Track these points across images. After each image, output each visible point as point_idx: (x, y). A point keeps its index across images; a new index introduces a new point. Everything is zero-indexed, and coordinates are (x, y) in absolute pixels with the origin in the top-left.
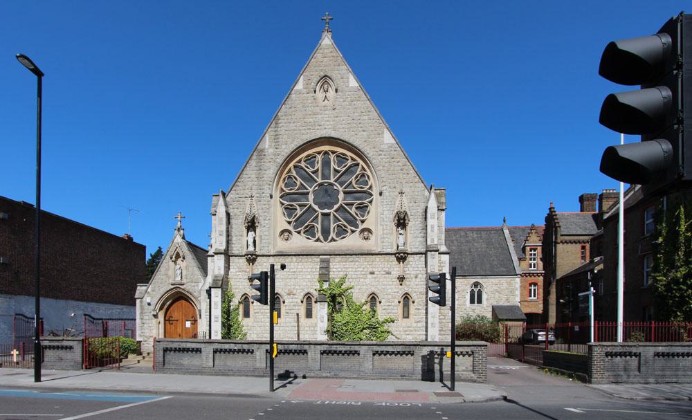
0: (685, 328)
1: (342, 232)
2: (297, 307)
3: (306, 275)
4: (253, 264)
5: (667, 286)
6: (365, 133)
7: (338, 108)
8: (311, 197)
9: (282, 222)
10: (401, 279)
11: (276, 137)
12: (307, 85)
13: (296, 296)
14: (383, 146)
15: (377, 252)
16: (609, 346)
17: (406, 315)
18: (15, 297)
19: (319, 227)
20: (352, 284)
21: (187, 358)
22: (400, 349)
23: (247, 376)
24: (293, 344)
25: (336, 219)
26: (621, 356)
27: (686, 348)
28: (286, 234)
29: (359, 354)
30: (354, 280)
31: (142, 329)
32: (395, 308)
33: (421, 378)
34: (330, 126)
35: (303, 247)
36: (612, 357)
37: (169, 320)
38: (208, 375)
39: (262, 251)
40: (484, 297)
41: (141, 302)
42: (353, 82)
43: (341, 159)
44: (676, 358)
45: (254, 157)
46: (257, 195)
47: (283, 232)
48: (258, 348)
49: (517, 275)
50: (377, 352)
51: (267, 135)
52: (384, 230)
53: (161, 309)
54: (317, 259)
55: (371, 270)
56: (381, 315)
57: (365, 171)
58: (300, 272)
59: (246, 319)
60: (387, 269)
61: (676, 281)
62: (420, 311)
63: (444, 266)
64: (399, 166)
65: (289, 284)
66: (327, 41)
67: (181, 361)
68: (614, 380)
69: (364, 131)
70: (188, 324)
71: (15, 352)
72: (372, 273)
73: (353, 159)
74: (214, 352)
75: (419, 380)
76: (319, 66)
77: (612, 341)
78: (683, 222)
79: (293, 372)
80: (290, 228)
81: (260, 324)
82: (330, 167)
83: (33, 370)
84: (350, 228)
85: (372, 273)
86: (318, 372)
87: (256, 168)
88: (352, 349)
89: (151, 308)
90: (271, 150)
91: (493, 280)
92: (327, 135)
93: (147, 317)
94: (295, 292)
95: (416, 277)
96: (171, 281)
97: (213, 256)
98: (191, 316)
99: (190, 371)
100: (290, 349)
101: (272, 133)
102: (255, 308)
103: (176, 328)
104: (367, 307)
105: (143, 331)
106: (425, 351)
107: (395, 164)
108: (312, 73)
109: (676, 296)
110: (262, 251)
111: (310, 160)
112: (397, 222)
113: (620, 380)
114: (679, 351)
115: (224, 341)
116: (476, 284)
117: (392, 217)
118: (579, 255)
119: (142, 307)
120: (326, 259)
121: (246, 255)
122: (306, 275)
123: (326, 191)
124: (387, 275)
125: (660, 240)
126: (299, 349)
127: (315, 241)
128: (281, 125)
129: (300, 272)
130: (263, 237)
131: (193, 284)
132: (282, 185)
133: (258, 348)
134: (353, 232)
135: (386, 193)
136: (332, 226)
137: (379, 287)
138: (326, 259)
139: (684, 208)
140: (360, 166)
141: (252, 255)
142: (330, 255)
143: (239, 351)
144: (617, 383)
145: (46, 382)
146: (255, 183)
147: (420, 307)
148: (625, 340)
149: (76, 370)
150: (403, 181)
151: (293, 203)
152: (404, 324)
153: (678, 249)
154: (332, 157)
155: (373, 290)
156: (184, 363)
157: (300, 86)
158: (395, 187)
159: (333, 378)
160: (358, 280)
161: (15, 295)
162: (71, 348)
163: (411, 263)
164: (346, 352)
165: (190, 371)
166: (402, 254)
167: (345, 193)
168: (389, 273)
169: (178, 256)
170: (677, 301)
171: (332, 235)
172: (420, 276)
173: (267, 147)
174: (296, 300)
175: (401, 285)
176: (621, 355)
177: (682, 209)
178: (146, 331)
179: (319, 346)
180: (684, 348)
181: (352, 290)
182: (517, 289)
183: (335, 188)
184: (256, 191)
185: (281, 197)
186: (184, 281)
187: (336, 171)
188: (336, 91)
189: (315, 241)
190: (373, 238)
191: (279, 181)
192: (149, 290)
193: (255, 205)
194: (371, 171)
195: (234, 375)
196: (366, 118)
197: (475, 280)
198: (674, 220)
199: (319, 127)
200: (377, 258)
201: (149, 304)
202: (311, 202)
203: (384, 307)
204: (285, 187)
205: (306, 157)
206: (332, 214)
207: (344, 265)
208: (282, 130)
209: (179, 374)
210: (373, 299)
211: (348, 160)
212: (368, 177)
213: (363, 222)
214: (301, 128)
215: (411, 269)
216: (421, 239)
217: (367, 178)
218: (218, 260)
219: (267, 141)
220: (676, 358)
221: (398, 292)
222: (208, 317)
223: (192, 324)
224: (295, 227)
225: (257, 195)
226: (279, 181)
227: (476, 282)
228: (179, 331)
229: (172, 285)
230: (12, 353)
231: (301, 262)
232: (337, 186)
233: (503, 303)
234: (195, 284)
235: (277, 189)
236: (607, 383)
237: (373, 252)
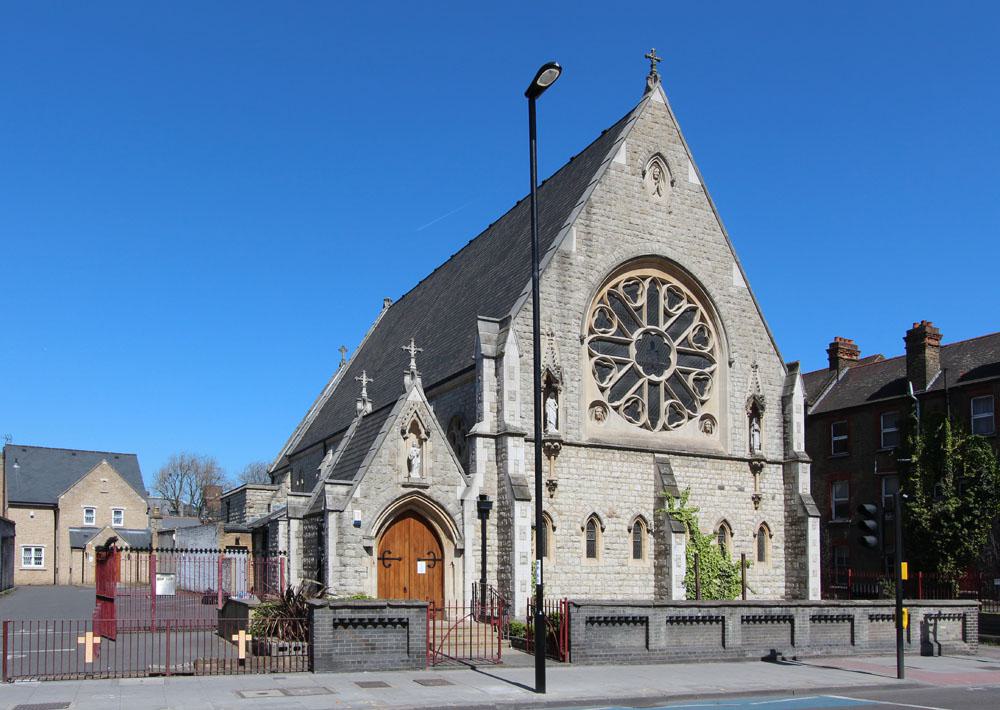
0: (957, 577)
1: (675, 415)
2: (622, 540)
3: (634, 484)
5: (935, 522)
6: (709, 263)
7: (675, 212)
9: (590, 389)
10: (757, 499)
11: (588, 238)
12: (632, 159)
13: (621, 520)
14: (732, 290)
15: (726, 455)
17: (761, 557)
19: (646, 402)
20: (697, 503)
21: (619, 636)
22: (759, 612)
23: (716, 661)
24: (775, 606)
25: (668, 395)
28: (600, 409)
30: (699, 498)
31: (341, 577)
32: (750, 544)
33: (919, 651)
34: (665, 240)
37: (435, 560)
38: (658, 663)
39: (569, 437)
41: (340, 519)
42: (694, 178)
43: (674, 296)
46: (561, 334)
47: (594, 404)
48: (731, 614)
50: (342, 621)
51: (574, 229)
54: (648, 458)
55: (719, 482)
57: (707, 322)
58: (626, 478)
60: (739, 483)
61: (945, 515)
62: (778, 550)
64: (751, 325)
65: (611, 498)
66: (657, 96)
67: (610, 641)
69: (708, 259)
70: (422, 567)
71: (89, 640)
72: (721, 488)
73: (690, 301)
75: (916, 654)
76: (648, 134)
78: (949, 440)
79: (780, 654)
80: (604, 398)
81: (566, 568)
82: (658, 306)
83: (534, 669)
84: (687, 411)
86: (807, 650)
87: (555, 284)
88: (825, 613)
89: (360, 532)
90: (581, 258)
93: (352, 553)
94: (618, 512)
95: (773, 498)
96: (402, 479)
98: (426, 552)
99: (630, 658)
100: (773, 614)
101: (582, 228)
102: (558, 538)
103: (397, 573)
104: (714, 542)
105: (343, 581)
108: (639, 143)
109: (947, 536)
110: (569, 437)
111: (632, 289)
112: (750, 411)
114: (831, 613)
115: (824, 602)
117: (744, 401)
119: (341, 532)
120: (663, 458)
122: (634, 484)
123: (652, 344)
124: (739, 493)
125: (915, 459)
126: (784, 614)
127: (641, 427)
128: (594, 217)
129: (626, 478)
130: (570, 411)
131: (446, 488)
133: (731, 614)
134: (690, 418)
135: (736, 364)
136: (628, 395)
137: (730, 511)
139: (951, 422)
140: (698, 314)
142: (668, 453)
143: (704, 620)
145: (555, 691)
146: (557, 311)
147: (778, 545)
149: (413, 669)
151: (608, 356)
152: (760, 571)
153: (945, 474)
155: (724, 515)
156: (616, 643)
158: (747, 357)
159: (825, 657)
160: (704, 497)
162: (404, 624)
163: (767, 476)
165: (630, 658)
166: (549, 444)
167: (679, 352)
168: (741, 490)
169: (415, 428)
170: (949, 543)
171: (663, 419)
172: (778, 497)
173: (574, 250)
174: (619, 527)
175: (756, 509)
177: (948, 424)
178: (350, 581)
179: (807, 609)
181: (697, 514)
183: (666, 341)
184: (558, 326)
186: (428, 480)
188: (672, 183)
189: (641, 427)
190: (717, 430)
192: (357, 494)
194: (715, 325)
195: (697, 661)
196: (710, 238)
198: (936, 436)
199: (648, 236)
200: (728, 464)
201: (357, 525)
202: (633, 359)
203: (737, 544)
204: (610, 325)
205: (675, 287)
206: (662, 386)
207: (686, 472)
208: (597, 227)
209: (613, 664)
210: (724, 529)
211: (682, 299)
212: (709, 332)
213: (703, 403)
214: (625, 232)
215: (767, 485)
216: (778, 441)
217: (706, 335)
218: (515, 446)
219: (575, 237)
222: (480, 553)
223: (429, 566)
225: (561, 334)
228: (404, 580)
229: (404, 486)
230: (81, 640)
234: (449, 488)
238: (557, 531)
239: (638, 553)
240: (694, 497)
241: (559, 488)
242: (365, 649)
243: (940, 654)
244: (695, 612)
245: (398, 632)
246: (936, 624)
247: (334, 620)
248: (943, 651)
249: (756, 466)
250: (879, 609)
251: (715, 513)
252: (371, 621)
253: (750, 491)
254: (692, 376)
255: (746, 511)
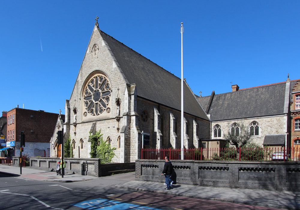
4: (119, 122)
8: (93, 97)
16: (143, 161)
18: (36, 143)
20: (103, 133)
26: (150, 167)
27: (183, 163)
29: (158, 167)
32: (116, 143)
35: (90, 118)
36: (146, 167)
40: (260, 130)
44: (180, 169)
45: (76, 85)
49: (284, 114)
52: (113, 107)
53: (56, 146)
56: (112, 147)
58: (88, 129)
59: (82, 149)
63: (133, 122)
68: (145, 179)
72: (109, 128)
74: (199, 168)
77: (179, 159)
85: (109, 128)
90: (80, 80)
91: (266, 119)
92: (95, 70)
97: (122, 117)
106: (82, 162)
107: (117, 76)
113: (247, 187)
114: (179, 165)
116: (254, 123)
118: (122, 118)
121: (116, 118)
132: (84, 94)
138: (94, 123)
141: (117, 118)
142: (96, 121)
144: (147, 181)
148: (185, 158)
150: (119, 84)
154: (98, 77)
157: (88, 52)
158: (116, 87)
161: (36, 142)
164: (256, 169)
167: (102, 93)
168: (114, 127)
176: (150, 166)
180: (182, 163)
182: (285, 124)
185: (84, 99)
187: (100, 84)
191: (83, 94)
193: (120, 94)
197: (216, 123)
204: (86, 94)
220: (180, 169)
221: (117, 136)
224: (88, 111)
226: (83, 94)
227: (254, 121)
231: (86, 125)
232: (100, 91)
233: (274, 134)
235: (82, 96)
236: (134, 180)
237: (110, 118)
238: (112, 141)
239: (218, 144)
240: (102, 131)
241: (77, 134)
242: (208, 175)
243: (86, 175)
244: (216, 165)
245: (248, 173)
246: (87, 166)
247: (199, 167)
248: (87, 174)
249: (118, 119)
250: (72, 160)
251: (107, 135)
252: (252, 169)
253: (116, 127)
254: (89, 102)
255: (115, 133)
